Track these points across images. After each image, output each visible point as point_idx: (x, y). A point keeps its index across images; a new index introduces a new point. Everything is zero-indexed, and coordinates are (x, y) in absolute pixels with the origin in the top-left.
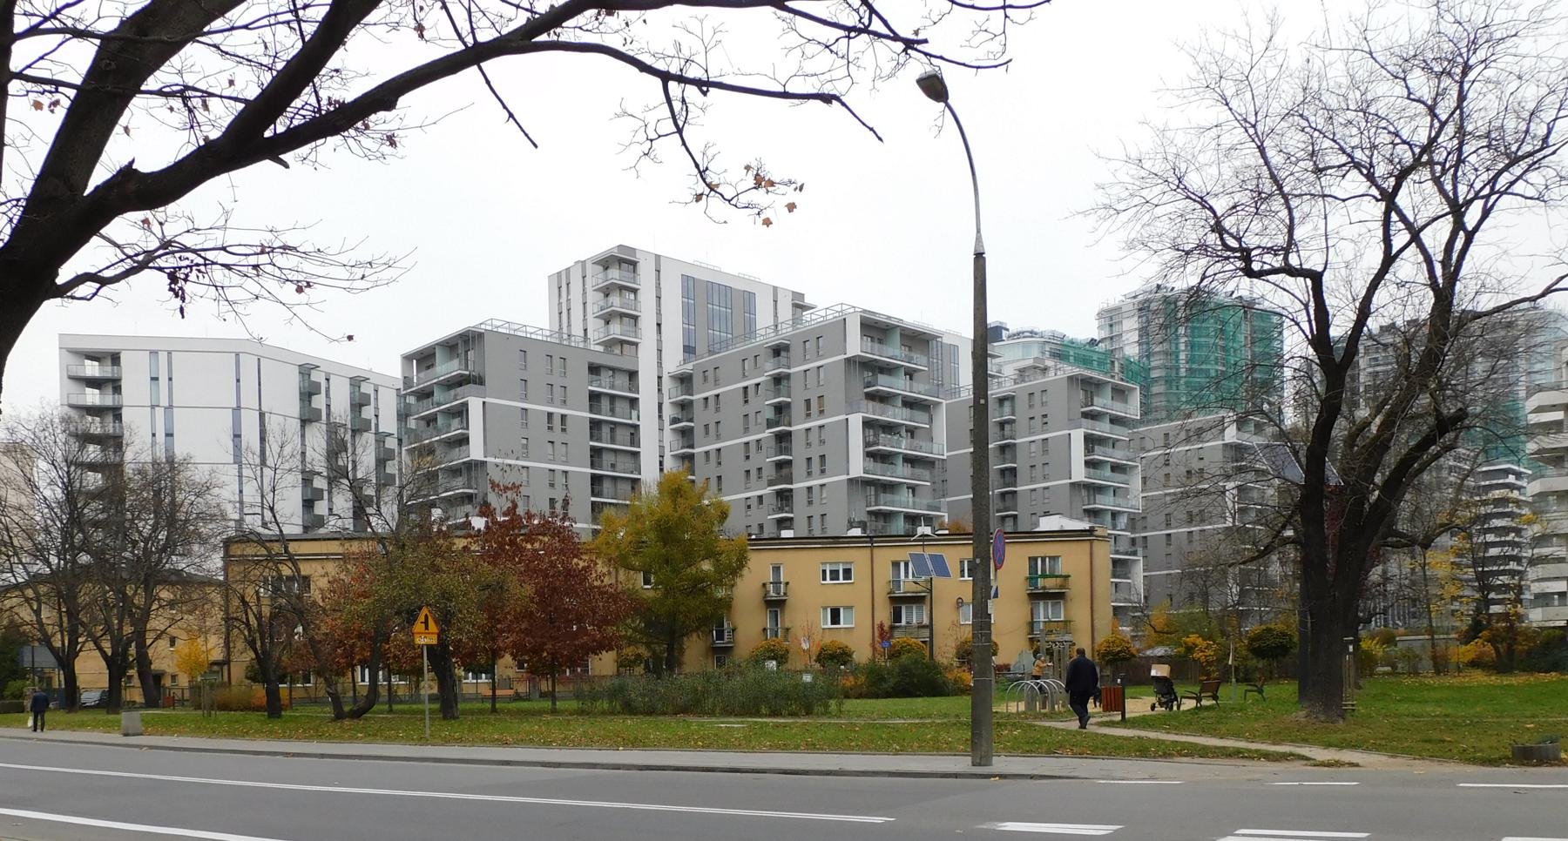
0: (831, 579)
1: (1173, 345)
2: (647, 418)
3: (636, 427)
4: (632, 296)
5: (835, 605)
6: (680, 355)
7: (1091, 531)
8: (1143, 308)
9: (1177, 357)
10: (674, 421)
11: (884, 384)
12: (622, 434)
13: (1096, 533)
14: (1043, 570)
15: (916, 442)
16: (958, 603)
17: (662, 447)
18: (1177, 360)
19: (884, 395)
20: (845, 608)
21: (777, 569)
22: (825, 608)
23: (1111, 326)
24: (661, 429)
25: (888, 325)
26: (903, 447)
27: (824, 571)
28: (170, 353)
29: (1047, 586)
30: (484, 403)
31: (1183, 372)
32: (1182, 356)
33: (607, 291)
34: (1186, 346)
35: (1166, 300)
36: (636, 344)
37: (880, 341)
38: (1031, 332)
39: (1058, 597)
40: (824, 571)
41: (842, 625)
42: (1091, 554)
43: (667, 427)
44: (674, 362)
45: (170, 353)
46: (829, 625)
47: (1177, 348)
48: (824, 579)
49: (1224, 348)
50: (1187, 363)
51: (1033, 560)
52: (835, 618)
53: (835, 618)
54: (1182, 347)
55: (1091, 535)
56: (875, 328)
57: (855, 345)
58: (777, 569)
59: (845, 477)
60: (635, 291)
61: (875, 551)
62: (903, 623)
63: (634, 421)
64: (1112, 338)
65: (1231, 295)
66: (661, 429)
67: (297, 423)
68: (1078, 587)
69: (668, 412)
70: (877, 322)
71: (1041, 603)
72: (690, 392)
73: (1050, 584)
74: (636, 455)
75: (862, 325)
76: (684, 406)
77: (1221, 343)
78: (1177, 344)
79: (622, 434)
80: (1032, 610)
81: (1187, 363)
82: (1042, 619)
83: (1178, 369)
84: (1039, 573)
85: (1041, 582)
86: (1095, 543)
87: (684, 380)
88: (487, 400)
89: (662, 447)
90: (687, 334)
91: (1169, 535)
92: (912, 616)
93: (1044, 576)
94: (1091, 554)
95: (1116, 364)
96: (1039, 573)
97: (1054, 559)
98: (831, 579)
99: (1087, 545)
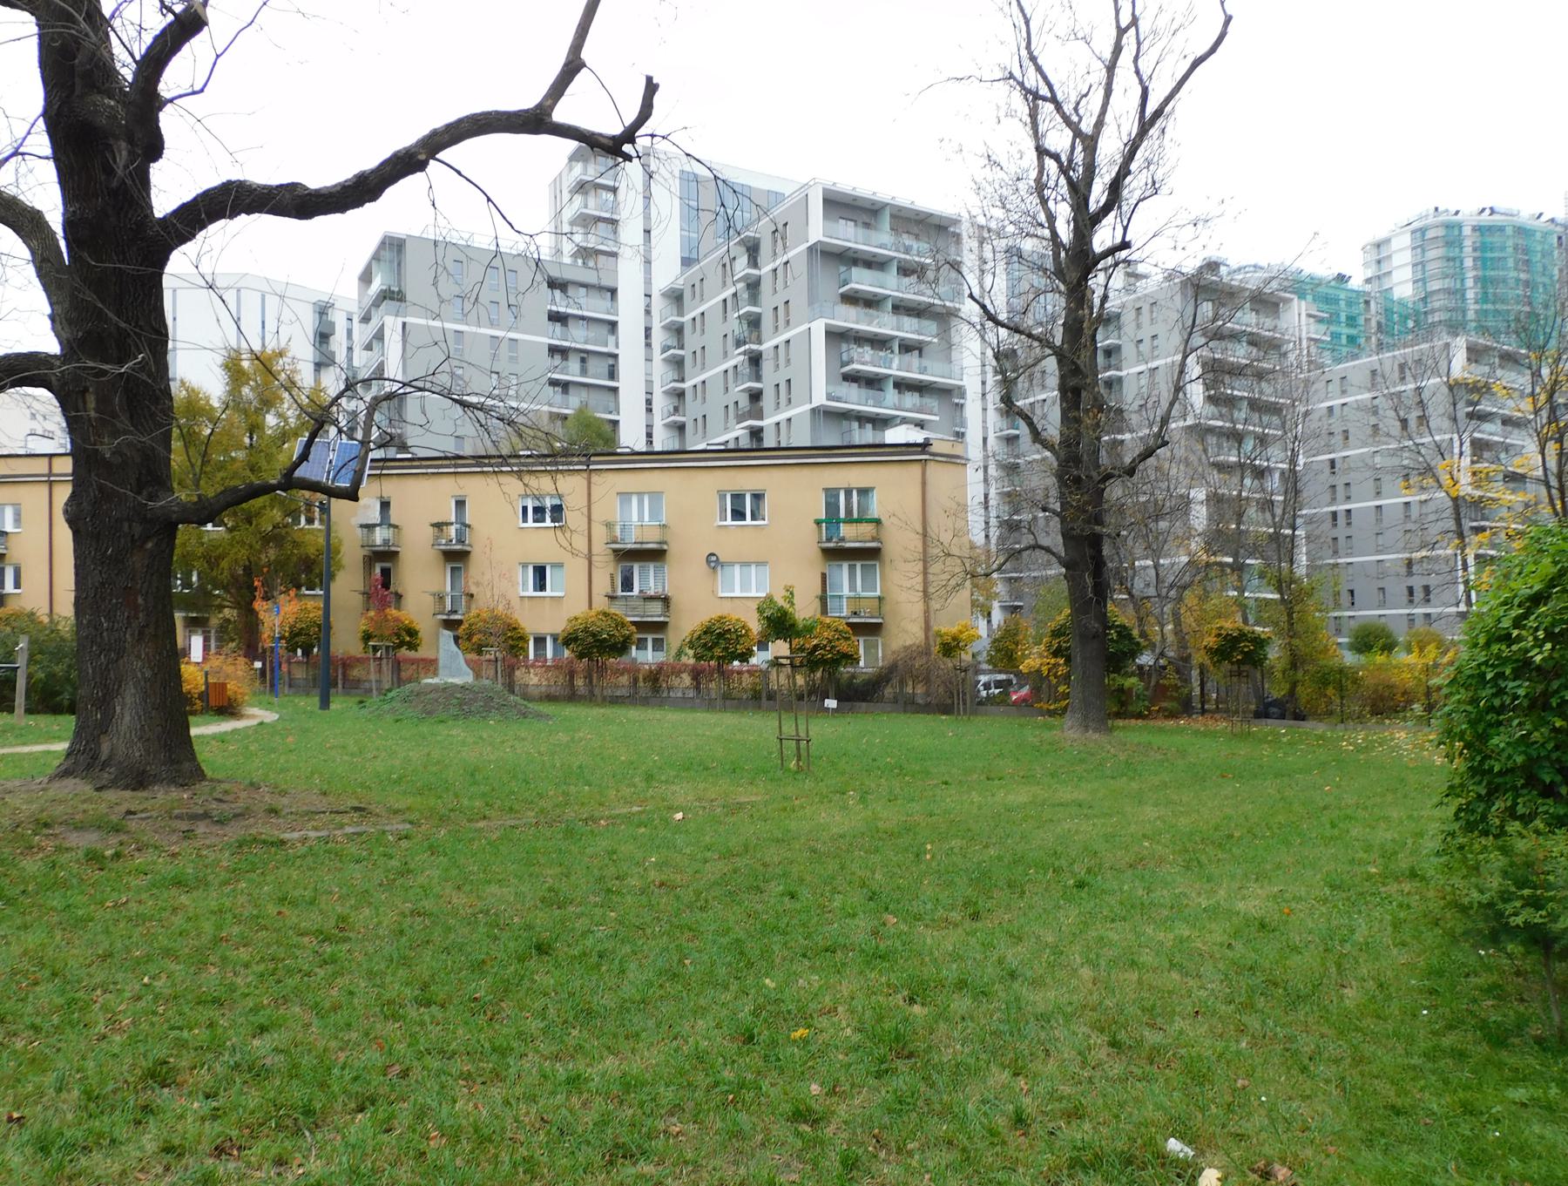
0: (535, 521)
1: (1458, 282)
2: (629, 345)
3: (615, 356)
4: (610, 196)
5: (540, 561)
6: (676, 266)
7: (924, 446)
8: (1420, 235)
9: (1463, 295)
10: (665, 349)
11: (863, 281)
12: (599, 367)
13: (933, 449)
14: (849, 511)
15: (925, 362)
16: (708, 562)
17: (649, 383)
18: (1464, 299)
19: (870, 297)
20: (554, 565)
21: (460, 504)
22: (525, 566)
23: (1379, 262)
24: (649, 360)
25: (874, 203)
26: (895, 366)
27: (525, 509)
28: (175, 291)
29: (847, 537)
30: (404, 324)
31: (1471, 315)
32: (1470, 295)
33: (582, 187)
34: (1475, 283)
35: (1448, 226)
36: (614, 255)
37: (867, 225)
38: (1255, 266)
39: (869, 555)
40: (525, 509)
41: (548, 593)
42: (924, 483)
43: (658, 356)
44: (667, 273)
45: (175, 291)
46: (531, 592)
47: (1462, 284)
48: (525, 520)
49: (1527, 284)
50: (1476, 303)
51: (831, 494)
52: (540, 584)
53: (540, 584)
54: (1469, 283)
55: (923, 453)
56: (839, 205)
57: (817, 229)
58: (460, 504)
59: (808, 407)
60: (614, 190)
61: (595, 478)
62: (636, 591)
63: (610, 349)
64: (1379, 277)
65: (1539, 217)
66: (649, 360)
67: (311, 367)
68: (901, 542)
69: (658, 337)
70: (855, 198)
71: (845, 566)
72: (681, 313)
73: (852, 535)
74: (615, 390)
75: (825, 200)
76: (678, 331)
77: (1523, 276)
78: (1463, 280)
79: (599, 367)
80: (824, 576)
81: (1476, 303)
82: (846, 591)
83: (1464, 312)
84: (842, 514)
85: (845, 530)
86: (931, 468)
87: (676, 298)
88: (409, 320)
89: (649, 383)
90: (686, 242)
91: (1379, 507)
92: (647, 580)
93: (849, 520)
94: (924, 483)
95: (1373, 304)
96: (842, 514)
97: (864, 492)
98: (535, 521)
99: (916, 470)
